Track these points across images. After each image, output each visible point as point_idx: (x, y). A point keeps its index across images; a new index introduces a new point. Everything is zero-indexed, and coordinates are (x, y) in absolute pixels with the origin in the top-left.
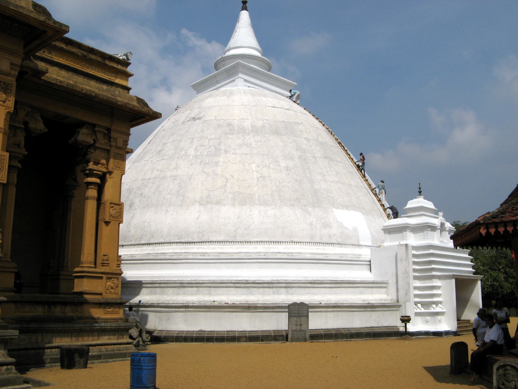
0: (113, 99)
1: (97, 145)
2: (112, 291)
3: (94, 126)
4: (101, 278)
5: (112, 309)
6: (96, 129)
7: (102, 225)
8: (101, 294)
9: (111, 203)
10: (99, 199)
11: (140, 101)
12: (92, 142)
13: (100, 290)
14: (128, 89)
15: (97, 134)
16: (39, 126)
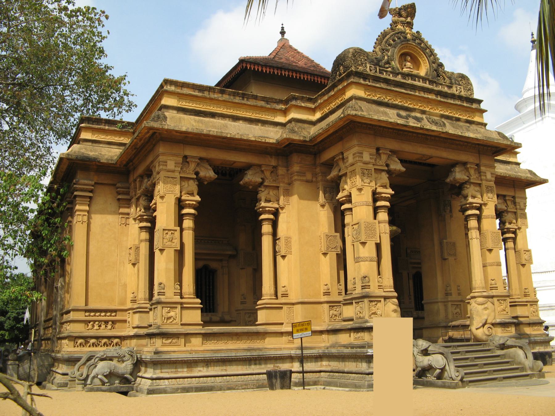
0: (516, 175)
1: (509, 210)
2: (534, 314)
3: (260, 166)
4: (527, 305)
5: (170, 341)
6: (507, 198)
7: (279, 258)
8: (528, 317)
9: (164, 230)
10: (274, 234)
11: (531, 172)
12: (261, 180)
13: (526, 314)
14: (518, 164)
15: (265, 172)
16: (208, 173)
